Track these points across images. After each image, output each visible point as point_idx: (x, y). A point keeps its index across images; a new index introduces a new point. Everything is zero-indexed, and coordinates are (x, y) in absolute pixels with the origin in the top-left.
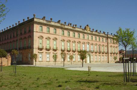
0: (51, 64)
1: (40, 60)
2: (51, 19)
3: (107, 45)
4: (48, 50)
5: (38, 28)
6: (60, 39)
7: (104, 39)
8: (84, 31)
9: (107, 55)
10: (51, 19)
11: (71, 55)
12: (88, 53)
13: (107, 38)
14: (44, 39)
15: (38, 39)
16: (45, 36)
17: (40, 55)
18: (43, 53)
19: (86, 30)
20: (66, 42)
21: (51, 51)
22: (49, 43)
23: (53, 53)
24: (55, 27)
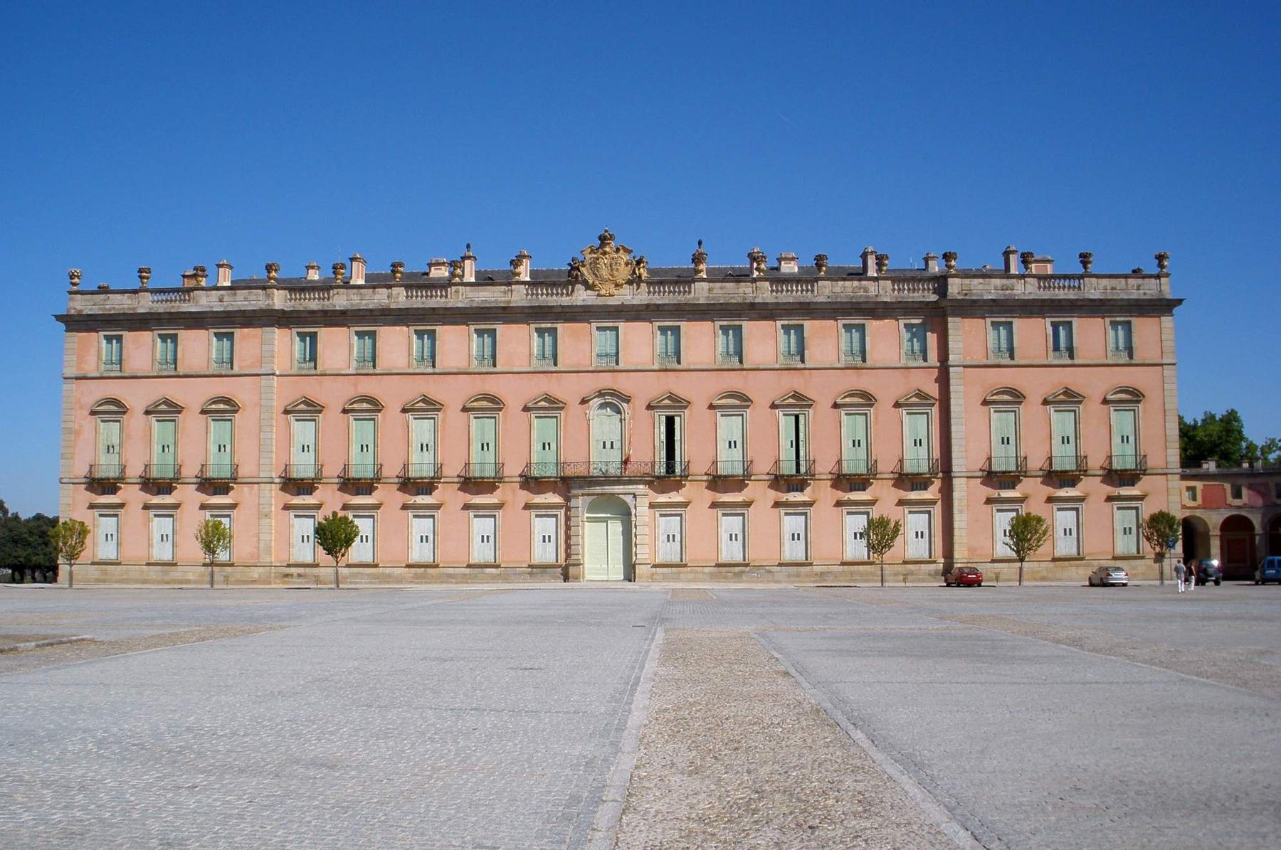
0: (188, 582)
1: (107, 551)
2: (1085, 259)
3: (933, 390)
4: (164, 487)
5: (93, 351)
6: (278, 404)
7: (888, 340)
8: (681, 299)
9: (932, 493)
10: (1085, 259)
11: (875, 513)
12: (598, 490)
13: (936, 315)
14: (136, 420)
15: (88, 423)
16: (1036, 384)
17: (108, 524)
18: (122, 506)
19: (589, 287)
20: (332, 416)
21: (188, 495)
22: (1129, 431)
23: (203, 507)
24: (483, 318)
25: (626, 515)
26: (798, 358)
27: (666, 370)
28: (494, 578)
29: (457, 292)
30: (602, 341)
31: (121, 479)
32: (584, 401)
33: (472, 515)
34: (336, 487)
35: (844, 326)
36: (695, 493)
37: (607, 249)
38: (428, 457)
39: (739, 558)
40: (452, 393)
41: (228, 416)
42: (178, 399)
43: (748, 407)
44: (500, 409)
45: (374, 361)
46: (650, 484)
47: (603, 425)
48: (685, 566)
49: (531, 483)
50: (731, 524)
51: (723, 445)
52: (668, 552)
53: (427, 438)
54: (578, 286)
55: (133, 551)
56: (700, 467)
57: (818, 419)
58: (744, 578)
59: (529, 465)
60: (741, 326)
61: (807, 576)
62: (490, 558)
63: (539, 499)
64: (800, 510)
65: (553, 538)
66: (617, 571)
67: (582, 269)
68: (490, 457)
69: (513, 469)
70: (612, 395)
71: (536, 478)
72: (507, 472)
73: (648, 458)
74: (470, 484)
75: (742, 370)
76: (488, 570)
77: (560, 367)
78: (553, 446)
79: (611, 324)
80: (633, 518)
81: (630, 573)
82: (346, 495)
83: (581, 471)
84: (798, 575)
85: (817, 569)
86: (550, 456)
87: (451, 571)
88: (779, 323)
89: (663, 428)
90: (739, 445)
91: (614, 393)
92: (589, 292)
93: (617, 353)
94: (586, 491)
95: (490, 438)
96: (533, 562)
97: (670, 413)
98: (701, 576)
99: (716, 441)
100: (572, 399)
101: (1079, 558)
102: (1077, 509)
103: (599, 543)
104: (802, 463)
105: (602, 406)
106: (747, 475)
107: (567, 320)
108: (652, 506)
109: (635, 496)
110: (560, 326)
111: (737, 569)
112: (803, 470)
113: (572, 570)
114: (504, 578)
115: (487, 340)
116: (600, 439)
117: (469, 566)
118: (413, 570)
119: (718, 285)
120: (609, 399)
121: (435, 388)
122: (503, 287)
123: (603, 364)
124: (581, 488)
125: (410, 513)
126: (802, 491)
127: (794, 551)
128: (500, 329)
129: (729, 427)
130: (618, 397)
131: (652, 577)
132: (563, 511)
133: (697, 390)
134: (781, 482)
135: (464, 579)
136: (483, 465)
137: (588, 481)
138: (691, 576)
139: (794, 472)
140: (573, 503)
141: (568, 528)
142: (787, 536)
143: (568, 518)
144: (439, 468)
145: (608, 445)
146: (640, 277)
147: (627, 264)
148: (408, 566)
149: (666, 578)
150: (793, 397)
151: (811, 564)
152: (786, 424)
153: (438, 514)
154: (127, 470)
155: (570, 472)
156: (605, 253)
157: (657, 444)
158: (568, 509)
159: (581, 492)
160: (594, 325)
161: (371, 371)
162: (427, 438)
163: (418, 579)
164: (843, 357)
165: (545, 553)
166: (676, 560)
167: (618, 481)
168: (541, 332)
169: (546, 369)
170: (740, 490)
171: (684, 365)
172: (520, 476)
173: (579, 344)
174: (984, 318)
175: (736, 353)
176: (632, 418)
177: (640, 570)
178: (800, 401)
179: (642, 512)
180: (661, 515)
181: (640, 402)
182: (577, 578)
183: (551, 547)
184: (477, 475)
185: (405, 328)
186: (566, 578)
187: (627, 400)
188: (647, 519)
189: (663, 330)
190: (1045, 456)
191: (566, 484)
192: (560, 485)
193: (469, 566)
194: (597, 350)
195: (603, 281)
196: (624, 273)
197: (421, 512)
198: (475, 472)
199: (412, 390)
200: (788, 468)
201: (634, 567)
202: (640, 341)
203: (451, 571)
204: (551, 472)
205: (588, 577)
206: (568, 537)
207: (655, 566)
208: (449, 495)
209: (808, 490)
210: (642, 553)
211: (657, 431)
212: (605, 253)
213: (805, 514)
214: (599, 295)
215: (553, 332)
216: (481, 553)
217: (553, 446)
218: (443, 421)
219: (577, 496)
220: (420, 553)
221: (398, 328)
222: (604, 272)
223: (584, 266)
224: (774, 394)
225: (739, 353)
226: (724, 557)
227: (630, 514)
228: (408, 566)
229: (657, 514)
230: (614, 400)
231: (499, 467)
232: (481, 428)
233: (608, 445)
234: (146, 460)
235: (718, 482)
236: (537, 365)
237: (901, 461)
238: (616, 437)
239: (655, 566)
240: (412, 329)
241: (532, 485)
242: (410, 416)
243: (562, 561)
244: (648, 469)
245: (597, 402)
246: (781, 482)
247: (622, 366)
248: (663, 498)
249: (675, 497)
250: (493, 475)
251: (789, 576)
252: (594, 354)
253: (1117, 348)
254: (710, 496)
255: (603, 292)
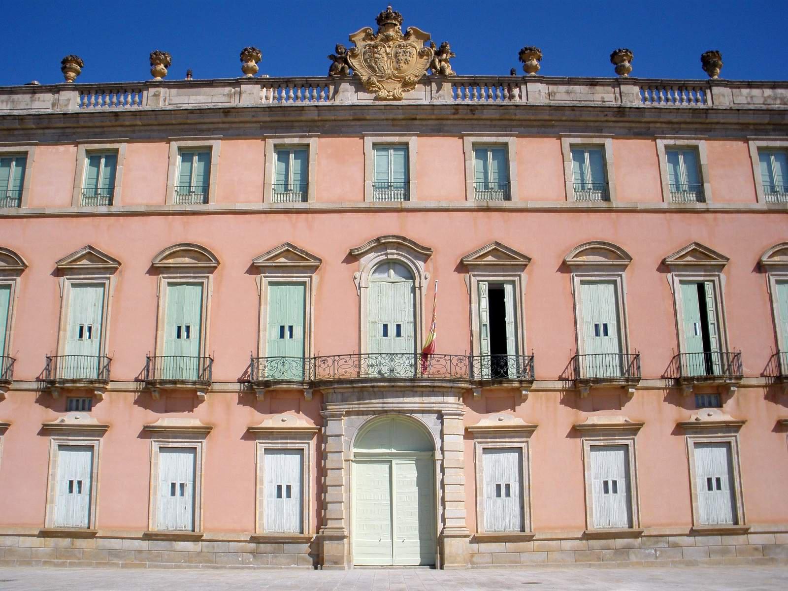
12: (376, 404)
19: (360, 86)
20: (134, 278)
25: (425, 452)
26: (501, 194)
27: (488, 209)
28: (190, 559)
29: (156, 95)
30: (383, 166)
31: (205, 384)
32: (352, 257)
33: (155, 446)
34: (132, 397)
35: (88, 152)
36: (545, 411)
37: (391, 33)
38: (90, 347)
39: (620, 522)
40: (135, 245)
41: (98, 278)
42: (104, 246)
43: (624, 267)
44: (211, 270)
45: (20, 199)
46: (466, 395)
47: (385, 299)
48: (530, 538)
49: (258, 392)
50: (606, 464)
51: (586, 331)
52: (500, 515)
53: (91, 317)
54: (345, 86)
55: (117, 513)
56: (550, 368)
57: (736, 285)
58: (633, 558)
59: (255, 361)
60: (603, 146)
61: (741, 552)
62: (184, 523)
63: (272, 421)
64: (720, 437)
65: (295, 490)
66: (409, 550)
67: (354, 62)
68: (190, 347)
69: (229, 370)
70: (398, 246)
71: (267, 384)
72: (218, 374)
73: (462, 349)
74: (156, 392)
75: (610, 210)
76: (180, 545)
77: (312, 204)
78: (298, 332)
79: (396, 139)
80: (438, 455)
81: (433, 555)
82: (149, 412)
83: (347, 370)
84: (724, 551)
85: (756, 540)
86: (293, 347)
87: (116, 544)
88: (661, 143)
89: (485, 303)
90: (612, 330)
91: (402, 243)
92: (361, 95)
93: (407, 182)
94: (354, 407)
95: (192, 318)
96: (260, 532)
97: (497, 278)
98: (556, 555)
99: (573, 324)
100: (333, 257)
101: (736, 529)
102: (728, 445)
103: (376, 499)
104: (715, 358)
105: (383, 266)
106: (205, 384)
107: (425, 132)
108: (469, 434)
109: (440, 416)
110: (314, 143)
111: (620, 542)
112: (717, 370)
113: (329, 548)
114: (210, 561)
115: (294, 163)
116: (379, 319)
117: (148, 537)
118: (51, 542)
119: (562, 88)
120: (393, 254)
121: (107, 237)
122: (227, 90)
123: (383, 200)
124: (344, 400)
125: (53, 442)
126: (720, 405)
127: (714, 509)
128: (219, 147)
129: (595, 301)
130: (410, 250)
131: (472, 561)
132: (313, 443)
133: (543, 242)
134: (680, 389)
135: (140, 560)
136: (177, 362)
137: (359, 388)
138: (541, 557)
139: (702, 372)
140: (332, 427)
141: (322, 472)
142: (700, 483)
143: (322, 455)
144: (106, 363)
145: (392, 330)
146: (442, 71)
147: (421, 55)
148: (45, 534)
149: (495, 561)
150: (693, 253)
151: (746, 532)
152: (687, 296)
153: (100, 444)
154: (16, 367)
155: (325, 372)
156: (388, 39)
157: (475, 328)
158: (322, 439)
159: (345, 407)
160: (369, 141)
161: (13, 211)
162: (91, 317)
163: (59, 558)
164: (668, 196)
165: (282, 517)
166: (514, 527)
167: (411, 387)
168: (283, 153)
169: (290, 206)
170: (619, 407)
171: (516, 201)
172: (241, 381)
173: (344, 168)
174: (77, 144)
175: (596, 187)
176: (432, 286)
177: (450, 546)
178: (703, 261)
179: (454, 446)
180: (486, 450)
181: (445, 260)
182: (337, 562)
183: (291, 505)
184: (168, 375)
185: (72, 148)
186: (318, 561)
187: (425, 254)
188: (461, 457)
189: (481, 150)
190: (768, 352)
191: (319, 394)
192: (307, 395)
193: (148, 537)
194: (373, 177)
195: (383, 77)
196: (416, 66)
197: (73, 441)
198: (164, 372)
199: (73, 238)
200: (694, 367)
201: (440, 541)
202: (444, 166)
203: (116, 544)
204: (293, 372)
205: (357, 559)
206: (322, 489)
207: (476, 540)
208: (118, 412)
209: (730, 404)
210: (455, 516)
211: (474, 306)
212: (388, 39)
213: (728, 445)
214: (376, 99)
215: (303, 152)
216: (172, 514)
217: (298, 332)
218: (118, 289)
219: (337, 416)
220: (67, 511)
221: (61, 148)
222: (387, 65)
223: (354, 56)
224: (667, 249)
225: (603, 187)
226: (596, 523)
227: (432, 449)
228: (45, 534)
229: (479, 448)
230: (401, 256)
231: (206, 363)
232: (179, 302)
233: (392, 330)
234: (148, 349)
235: (580, 391)
236: (274, 200)
237: (575, 359)
238: (405, 318)
239: (476, 540)
240: (83, 148)
241: (260, 396)
242: (65, 282)
243: (310, 531)
244: (461, 370)
245: (371, 260)
246: (680, 389)
247: (414, 202)
248: (489, 421)
249: (508, 419)
250: (194, 377)
251: (709, 553)
252: (369, 184)
253: (486, 184)
254: (568, 416)
255: (383, 93)
